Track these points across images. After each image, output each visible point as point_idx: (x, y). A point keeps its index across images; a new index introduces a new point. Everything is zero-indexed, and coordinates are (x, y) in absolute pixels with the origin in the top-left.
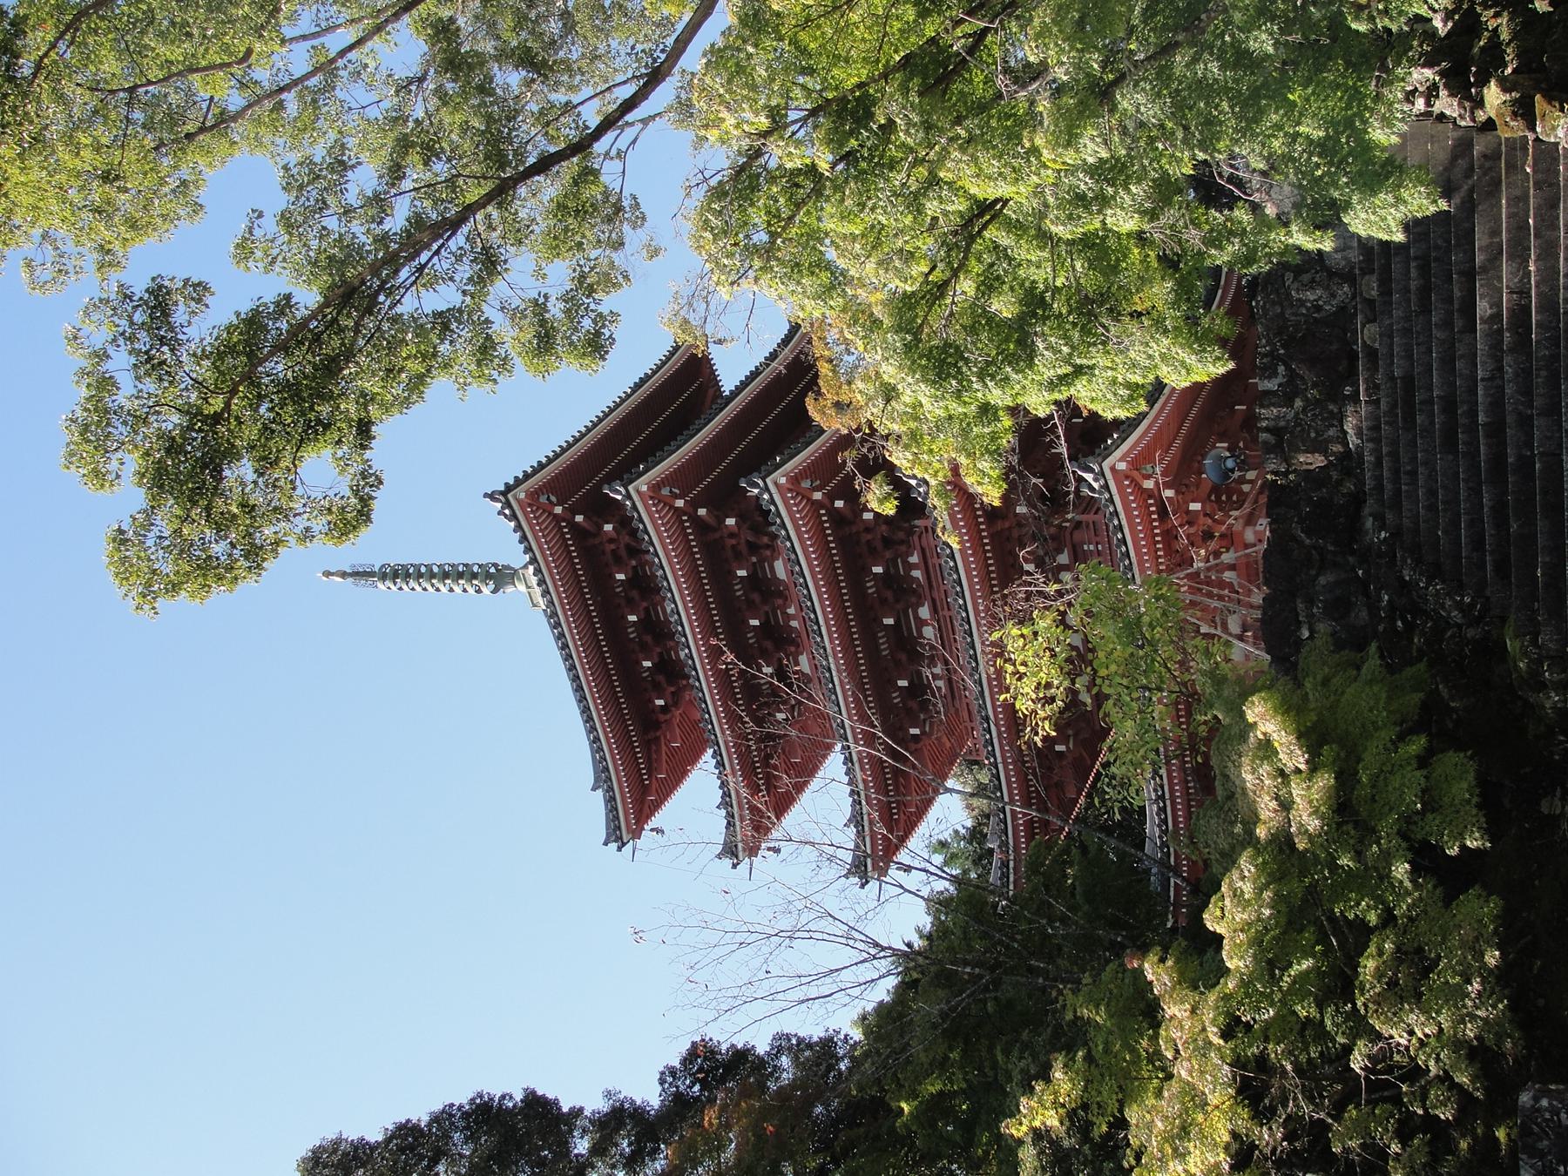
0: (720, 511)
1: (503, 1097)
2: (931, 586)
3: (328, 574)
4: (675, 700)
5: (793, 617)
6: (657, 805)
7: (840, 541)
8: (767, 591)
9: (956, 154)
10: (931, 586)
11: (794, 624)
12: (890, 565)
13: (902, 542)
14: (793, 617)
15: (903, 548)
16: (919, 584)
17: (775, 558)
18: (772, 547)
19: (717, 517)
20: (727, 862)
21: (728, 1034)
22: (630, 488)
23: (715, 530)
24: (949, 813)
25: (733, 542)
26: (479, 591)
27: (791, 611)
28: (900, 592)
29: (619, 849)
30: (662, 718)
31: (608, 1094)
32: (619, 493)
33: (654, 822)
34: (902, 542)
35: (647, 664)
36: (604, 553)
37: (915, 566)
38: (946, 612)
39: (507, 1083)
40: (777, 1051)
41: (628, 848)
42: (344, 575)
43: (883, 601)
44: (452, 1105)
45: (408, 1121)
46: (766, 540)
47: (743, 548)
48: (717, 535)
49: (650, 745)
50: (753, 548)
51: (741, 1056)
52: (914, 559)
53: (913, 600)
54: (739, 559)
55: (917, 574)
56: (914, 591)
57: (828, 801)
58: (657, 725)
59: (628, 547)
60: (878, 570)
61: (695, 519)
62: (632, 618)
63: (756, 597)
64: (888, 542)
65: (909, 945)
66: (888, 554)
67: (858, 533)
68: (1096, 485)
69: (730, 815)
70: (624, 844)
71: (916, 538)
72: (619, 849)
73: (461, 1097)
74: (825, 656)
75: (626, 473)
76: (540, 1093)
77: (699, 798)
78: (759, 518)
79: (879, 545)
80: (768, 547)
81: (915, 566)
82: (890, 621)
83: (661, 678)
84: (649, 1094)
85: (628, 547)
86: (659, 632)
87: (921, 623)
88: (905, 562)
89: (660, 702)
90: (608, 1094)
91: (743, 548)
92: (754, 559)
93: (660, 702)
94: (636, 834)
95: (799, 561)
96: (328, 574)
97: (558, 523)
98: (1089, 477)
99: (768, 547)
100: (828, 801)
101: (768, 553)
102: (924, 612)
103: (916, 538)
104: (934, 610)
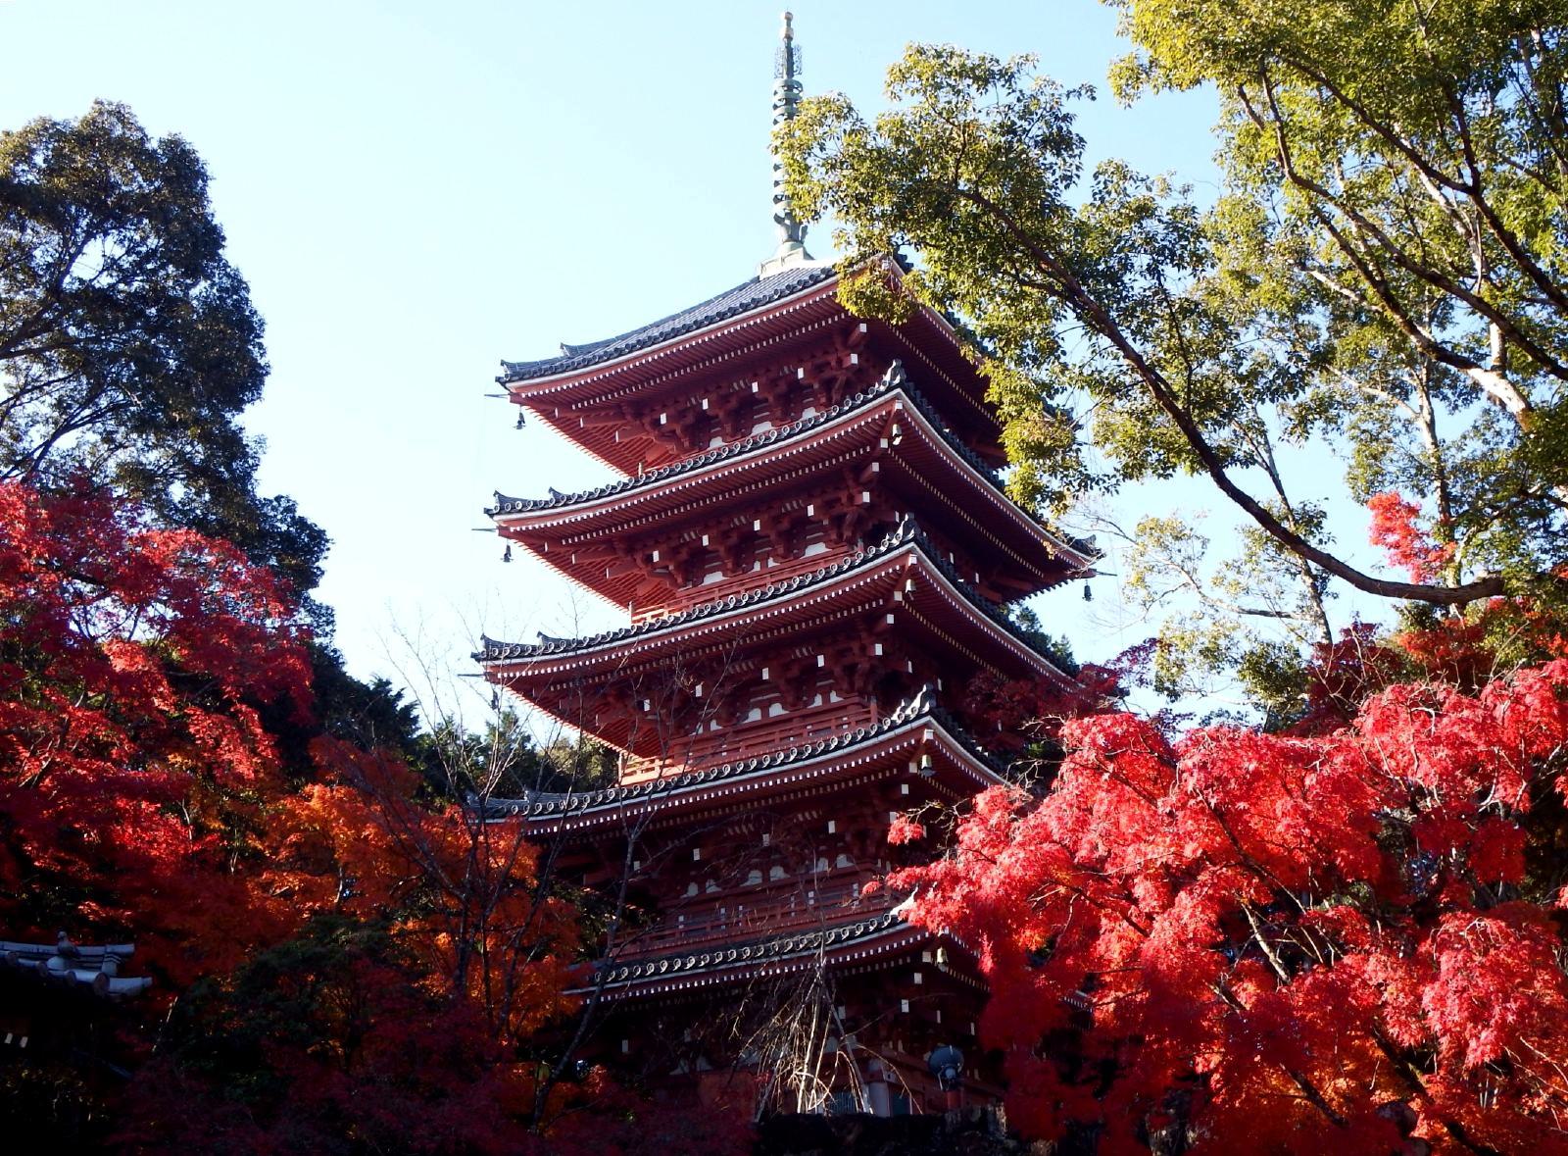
0: (875, 485)
1: (260, 346)
2: (804, 717)
3: (789, 19)
4: (668, 435)
5: (764, 565)
6: (548, 416)
7: (851, 620)
8: (793, 536)
9: (1168, 840)
10: (804, 717)
11: (757, 567)
12: (826, 673)
13: (852, 684)
14: (764, 565)
15: (845, 686)
16: (806, 704)
17: (828, 543)
18: (828, 404)
19: (870, 481)
20: (493, 503)
21: (329, 563)
22: (912, 544)
23: (856, 480)
24: (544, 731)
25: (844, 500)
26: (777, 167)
27: (771, 563)
28: (800, 684)
29: (498, 380)
30: (647, 420)
31: (260, 442)
32: (893, 378)
33: (530, 415)
34: (852, 684)
35: (705, 405)
36: (826, 353)
37: (826, 699)
38: (777, 736)
39: (276, 347)
40: (315, 611)
41: (499, 389)
42: (789, 38)
43: (787, 667)
44: (247, 289)
45: (224, 238)
46: (847, 534)
47: (827, 374)
48: (850, 483)
49: (617, 410)
50: (828, 385)
51: (310, 578)
52: (834, 698)
53: (790, 699)
54: (824, 508)
55: (818, 701)
56: (799, 699)
57: (584, 615)
58: (638, 415)
59: (834, 379)
60: (821, 661)
61: (867, 460)
62: (755, 387)
63: (785, 525)
64: (862, 836)
65: (399, 696)
66: (837, 670)
67: (848, 487)
68: (908, 711)
69: (545, 505)
70: (503, 384)
71: (857, 699)
72: (498, 380)
73: (260, 300)
74: (727, 601)
75: (918, 384)
76: (267, 379)
77: (577, 472)
78: (860, 382)
79: (847, 660)
80: (840, 536)
81: (826, 699)
82: (766, 676)
83: (690, 419)
84: (265, 486)
85: (834, 379)
86: (740, 417)
87: (765, 707)
88: (830, 688)
89: (663, 419)
90: (260, 442)
91: (837, 510)
92: (826, 522)
93: (663, 419)
94: (515, 398)
95: (843, 740)
96: (789, 19)
97: (870, 443)
98: (917, 703)
99: (840, 536)
100: (584, 615)
101: (834, 537)
102: (776, 710)
103: (857, 699)
104: (779, 721)
